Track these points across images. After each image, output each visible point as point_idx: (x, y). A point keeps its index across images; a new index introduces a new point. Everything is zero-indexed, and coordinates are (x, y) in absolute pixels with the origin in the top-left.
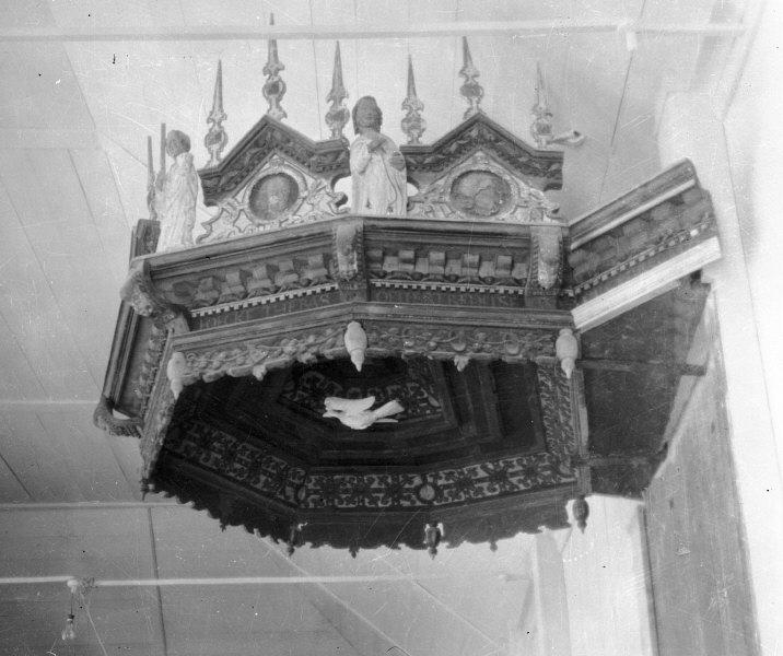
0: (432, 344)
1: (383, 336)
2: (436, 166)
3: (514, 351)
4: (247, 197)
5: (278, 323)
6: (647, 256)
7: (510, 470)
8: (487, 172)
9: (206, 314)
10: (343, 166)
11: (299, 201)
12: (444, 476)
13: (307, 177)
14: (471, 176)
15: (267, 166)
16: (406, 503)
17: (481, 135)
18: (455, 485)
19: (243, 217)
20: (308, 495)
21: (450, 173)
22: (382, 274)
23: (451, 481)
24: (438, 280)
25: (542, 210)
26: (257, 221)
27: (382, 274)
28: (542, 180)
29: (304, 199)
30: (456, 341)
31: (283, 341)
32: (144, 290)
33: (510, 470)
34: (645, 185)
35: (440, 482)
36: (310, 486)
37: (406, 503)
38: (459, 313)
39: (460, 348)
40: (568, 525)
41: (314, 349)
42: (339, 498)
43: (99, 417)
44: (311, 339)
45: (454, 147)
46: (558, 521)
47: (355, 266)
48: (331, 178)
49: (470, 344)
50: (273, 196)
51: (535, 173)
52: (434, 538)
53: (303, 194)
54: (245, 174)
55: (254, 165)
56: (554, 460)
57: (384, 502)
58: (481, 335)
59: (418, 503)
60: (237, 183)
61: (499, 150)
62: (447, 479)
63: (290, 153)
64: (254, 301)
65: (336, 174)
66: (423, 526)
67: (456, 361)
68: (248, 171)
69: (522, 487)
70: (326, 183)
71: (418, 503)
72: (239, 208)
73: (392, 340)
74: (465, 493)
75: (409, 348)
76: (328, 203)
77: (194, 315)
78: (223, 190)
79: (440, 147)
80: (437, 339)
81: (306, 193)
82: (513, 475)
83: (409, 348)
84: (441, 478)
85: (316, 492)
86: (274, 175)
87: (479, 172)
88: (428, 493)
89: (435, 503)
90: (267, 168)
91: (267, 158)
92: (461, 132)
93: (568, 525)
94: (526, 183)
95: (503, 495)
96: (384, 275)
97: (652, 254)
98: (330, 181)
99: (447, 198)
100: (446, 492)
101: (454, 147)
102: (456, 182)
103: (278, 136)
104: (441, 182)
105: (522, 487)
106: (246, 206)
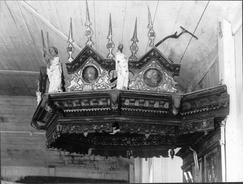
0: (139, 130)
1: (124, 127)
2: (140, 67)
3: (163, 133)
4: (81, 73)
5: (92, 119)
6: (206, 110)
7: (153, 139)
8: (156, 69)
9: (68, 112)
10: (113, 67)
11: (98, 78)
12: (134, 138)
13: (101, 69)
14: (150, 70)
15: (88, 62)
16: (122, 145)
17: (154, 55)
18: (137, 141)
19: (80, 80)
20: (94, 141)
21: (144, 69)
22: (124, 106)
23: (136, 140)
24: (141, 109)
25: (172, 85)
26: (85, 83)
27: (124, 106)
28: (173, 73)
29: (100, 77)
30: (146, 129)
31: (93, 125)
32: (49, 105)
33: (153, 139)
34: (210, 89)
35: (132, 140)
36: (95, 139)
37: (122, 145)
38: (147, 120)
39: (147, 131)
40: (168, 157)
41: (103, 129)
42: (103, 142)
43: (33, 124)
44: (102, 126)
45: (145, 60)
46: (166, 155)
47: (117, 108)
48: (109, 71)
49: (150, 130)
50: (90, 74)
51: (171, 70)
52: (130, 155)
53: (100, 75)
54: (81, 65)
55: (84, 62)
56: (166, 138)
57: (116, 144)
58: (153, 127)
59: (126, 145)
60: (78, 68)
61: (160, 61)
62: (134, 139)
63: (95, 59)
64: (84, 110)
65: (110, 70)
66: (127, 151)
67: (146, 135)
68: (82, 64)
69: (156, 144)
70: (107, 72)
71: (126, 145)
72: (79, 77)
73: (127, 128)
74: (139, 144)
75: (132, 131)
76: (108, 80)
77: (65, 112)
78: (74, 70)
79: (142, 60)
80: (140, 128)
81: (100, 75)
82: (154, 141)
83: (132, 131)
84: (133, 139)
85: (96, 140)
86: (90, 66)
87: (153, 69)
88: (129, 142)
89: (130, 145)
90: (88, 63)
91: (88, 60)
92: (148, 54)
93: (168, 157)
94: (168, 74)
95: (151, 145)
96: (125, 106)
97: (208, 110)
98: (108, 72)
99: (142, 80)
100: (134, 143)
101: (145, 60)
102: (146, 73)
103: (91, 52)
104: (141, 73)
105: (156, 144)
106: (81, 77)
